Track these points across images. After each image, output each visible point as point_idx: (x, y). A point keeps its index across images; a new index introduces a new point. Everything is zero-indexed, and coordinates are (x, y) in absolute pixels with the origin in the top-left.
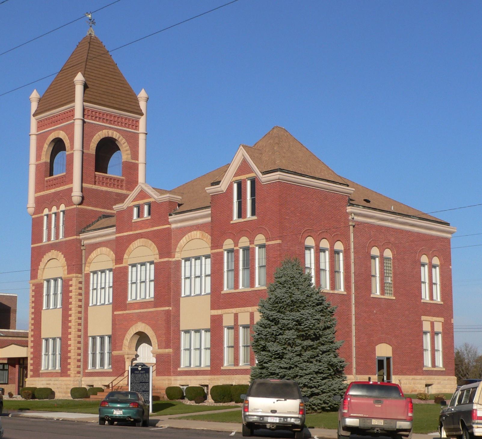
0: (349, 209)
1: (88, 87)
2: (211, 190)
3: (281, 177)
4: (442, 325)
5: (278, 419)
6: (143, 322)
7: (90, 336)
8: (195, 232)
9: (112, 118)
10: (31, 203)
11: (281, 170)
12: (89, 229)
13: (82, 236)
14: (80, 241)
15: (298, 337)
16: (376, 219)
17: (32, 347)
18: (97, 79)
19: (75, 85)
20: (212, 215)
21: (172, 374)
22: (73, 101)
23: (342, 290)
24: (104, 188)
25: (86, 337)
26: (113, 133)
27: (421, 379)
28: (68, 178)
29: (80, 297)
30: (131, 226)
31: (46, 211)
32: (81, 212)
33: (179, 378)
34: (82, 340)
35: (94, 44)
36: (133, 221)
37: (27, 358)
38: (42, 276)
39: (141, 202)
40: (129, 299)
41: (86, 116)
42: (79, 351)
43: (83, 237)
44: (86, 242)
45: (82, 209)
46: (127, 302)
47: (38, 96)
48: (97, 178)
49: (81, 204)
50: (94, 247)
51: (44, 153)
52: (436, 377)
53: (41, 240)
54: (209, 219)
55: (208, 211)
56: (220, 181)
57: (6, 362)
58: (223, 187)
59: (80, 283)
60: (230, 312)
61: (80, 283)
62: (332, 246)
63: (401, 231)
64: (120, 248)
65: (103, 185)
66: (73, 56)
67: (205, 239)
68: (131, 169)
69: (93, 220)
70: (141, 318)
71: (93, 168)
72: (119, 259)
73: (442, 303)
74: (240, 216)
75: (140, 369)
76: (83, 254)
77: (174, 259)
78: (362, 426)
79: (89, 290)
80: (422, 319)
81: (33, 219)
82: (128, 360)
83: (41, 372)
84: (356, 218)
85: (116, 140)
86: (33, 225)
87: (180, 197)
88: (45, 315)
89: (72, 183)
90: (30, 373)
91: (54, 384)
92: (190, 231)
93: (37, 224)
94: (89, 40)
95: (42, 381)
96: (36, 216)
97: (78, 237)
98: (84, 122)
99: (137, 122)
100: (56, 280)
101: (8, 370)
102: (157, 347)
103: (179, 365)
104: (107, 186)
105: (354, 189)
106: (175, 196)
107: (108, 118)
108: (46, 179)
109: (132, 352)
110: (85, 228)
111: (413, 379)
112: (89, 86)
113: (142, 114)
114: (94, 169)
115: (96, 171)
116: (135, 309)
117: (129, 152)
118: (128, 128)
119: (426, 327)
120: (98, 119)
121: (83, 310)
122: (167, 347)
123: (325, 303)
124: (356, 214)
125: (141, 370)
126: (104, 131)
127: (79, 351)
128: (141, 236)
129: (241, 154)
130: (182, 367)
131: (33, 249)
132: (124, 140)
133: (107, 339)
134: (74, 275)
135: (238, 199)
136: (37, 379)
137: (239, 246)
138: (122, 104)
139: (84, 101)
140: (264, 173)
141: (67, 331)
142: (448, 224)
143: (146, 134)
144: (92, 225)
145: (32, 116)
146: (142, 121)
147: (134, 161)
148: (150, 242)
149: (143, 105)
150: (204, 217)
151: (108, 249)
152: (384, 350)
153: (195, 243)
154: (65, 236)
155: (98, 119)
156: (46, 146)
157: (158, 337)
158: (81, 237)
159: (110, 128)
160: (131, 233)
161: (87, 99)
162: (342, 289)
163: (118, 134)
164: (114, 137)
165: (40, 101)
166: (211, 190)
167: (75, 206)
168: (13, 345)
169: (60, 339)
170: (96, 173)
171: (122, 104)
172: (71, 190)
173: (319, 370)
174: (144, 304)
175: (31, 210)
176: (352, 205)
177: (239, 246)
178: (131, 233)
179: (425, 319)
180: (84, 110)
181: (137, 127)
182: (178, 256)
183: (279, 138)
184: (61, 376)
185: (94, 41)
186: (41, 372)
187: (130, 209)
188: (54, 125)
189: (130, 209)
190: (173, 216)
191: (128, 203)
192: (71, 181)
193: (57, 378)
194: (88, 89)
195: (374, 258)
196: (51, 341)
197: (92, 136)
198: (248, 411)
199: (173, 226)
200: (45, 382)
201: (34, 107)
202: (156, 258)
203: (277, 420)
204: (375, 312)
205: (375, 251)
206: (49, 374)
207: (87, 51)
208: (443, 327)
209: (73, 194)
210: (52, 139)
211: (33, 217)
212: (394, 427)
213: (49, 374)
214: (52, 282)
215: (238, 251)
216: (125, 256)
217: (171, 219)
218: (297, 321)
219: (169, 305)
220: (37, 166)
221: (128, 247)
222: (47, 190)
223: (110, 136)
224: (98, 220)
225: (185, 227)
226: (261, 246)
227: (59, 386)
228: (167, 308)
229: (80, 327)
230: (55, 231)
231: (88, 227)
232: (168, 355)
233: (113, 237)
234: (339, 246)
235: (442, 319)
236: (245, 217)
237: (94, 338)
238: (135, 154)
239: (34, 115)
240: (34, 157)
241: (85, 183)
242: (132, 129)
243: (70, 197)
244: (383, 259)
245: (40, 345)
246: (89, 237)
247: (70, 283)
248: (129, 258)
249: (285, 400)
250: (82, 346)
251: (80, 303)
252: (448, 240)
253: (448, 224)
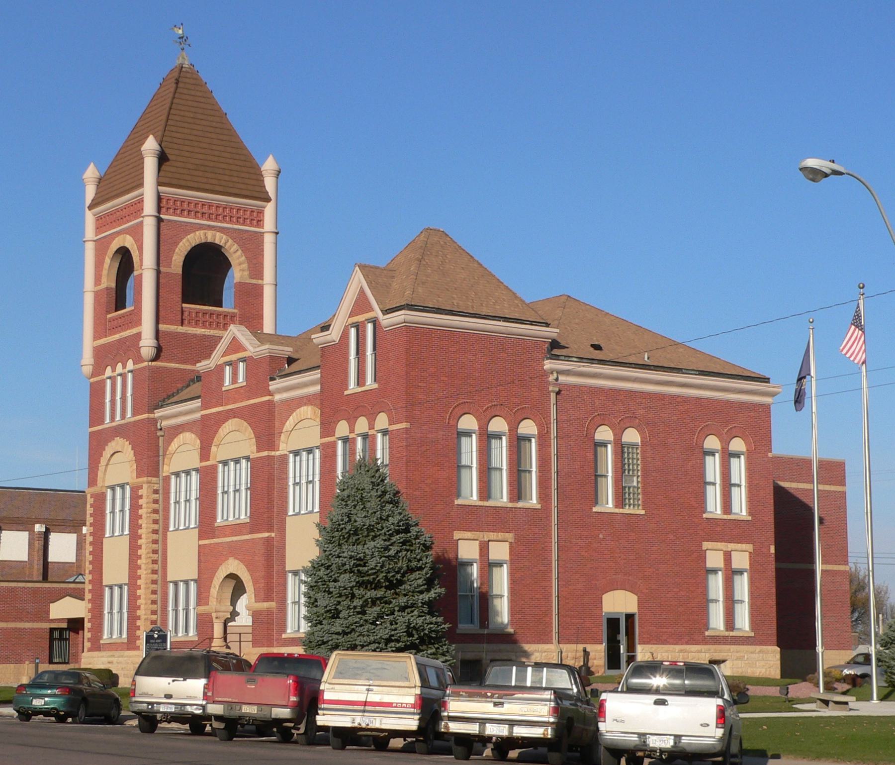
0: (548, 365)
1: (167, 160)
2: (319, 338)
3: (409, 318)
4: (750, 557)
5: (173, 707)
6: (236, 558)
7: (171, 582)
8: (305, 408)
9: (213, 210)
10: (87, 358)
11: (410, 307)
12: (170, 401)
13: (158, 413)
14: (154, 421)
15: (360, 585)
16: (606, 378)
17: (89, 600)
18: (187, 142)
19: (143, 158)
20: (322, 382)
21: (275, 643)
22: (141, 185)
23: (533, 501)
24: (199, 331)
25: (165, 583)
26: (214, 236)
27: (700, 652)
28: (135, 319)
29: (156, 516)
30: (220, 397)
31: (109, 372)
32: (155, 371)
34: (158, 587)
35: (187, 80)
36: (224, 389)
37: (83, 619)
38: (104, 481)
39: (234, 357)
40: (219, 520)
41: (163, 210)
42: (154, 607)
43: (160, 414)
44: (165, 423)
45: (158, 368)
46: (216, 525)
47: (97, 175)
48: (186, 314)
49: (156, 358)
50: (177, 430)
51: (105, 272)
52: (733, 648)
53: (101, 421)
54: (317, 388)
55: (316, 375)
56: (330, 326)
57: (65, 625)
58: (334, 334)
59: (156, 492)
61: (156, 492)
62: (513, 428)
63: (661, 397)
64: (207, 431)
65: (197, 325)
66: (155, 102)
68: (251, 295)
69: (180, 386)
70: (234, 551)
71: (178, 297)
72: (205, 453)
73: (750, 518)
75: (156, 636)
77: (278, 453)
78: (227, 714)
79: (169, 503)
80: (704, 548)
81: (91, 384)
82: (218, 621)
83: (102, 642)
84: (562, 379)
85: (221, 247)
86: (92, 395)
87: (291, 349)
88: (108, 545)
89: (141, 325)
90: (87, 645)
91: (118, 663)
92: (299, 406)
93: (97, 392)
94: (176, 75)
95: (102, 657)
97: (151, 416)
98: (159, 220)
99: (261, 212)
100: (122, 486)
101: (68, 639)
103: (283, 628)
104: (204, 326)
105: (558, 331)
106: (281, 348)
107: (205, 210)
108: (109, 316)
109: (223, 608)
110: (164, 400)
111: (681, 651)
112: (169, 157)
113: (268, 200)
114: (180, 300)
115: (184, 301)
116: (225, 536)
117: (245, 266)
118: (243, 224)
119: (714, 559)
120: (186, 213)
121: (159, 537)
122: (268, 599)
123: (414, 530)
124: (560, 372)
125: (158, 638)
126: (197, 233)
127: (154, 607)
129: (358, 280)
130: (289, 631)
131: (92, 434)
132: (235, 247)
133: (193, 586)
134: (145, 479)
136: (96, 653)
137: (337, 435)
138: (231, 185)
139: (159, 184)
140: (386, 312)
142: (766, 380)
143: (277, 233)
144: (178, 393)
145: (87, 209)
146: (269, 210)
147: (254, 281)
148: (245, 424)
149: (269, 184)
150: (309, 383)
151: (193, 436)
152: (619, 602)
153: (302, 430)
154: (134, 415)
155: (186, 213)
156: (108, 260)
157: (255, 582)
158: (156, 415)
159: (210, 228)
160: (220, 409)
161: (163, 180)
162: (534, 501)
163: (224, 237)
164: (217, 242)
165: (100, 181)
166: (319, 338)
167: (146, 364)
168: (68, 598)
169: (195, 581)
170: (184, 305)
171: (231, 185)
172: (138, 336)
173: (393, 635)
174: (237, 529)
175: (87, 370)
176: (557, 357)
177: (337, 435)
178: (220, 409)
179: (710, 547)
180: (159, 199)
181: (260, 222)
182: (283, 448)
183: (433, 248)
184: (128, 649)
185: (188, 75)
186: (102, 642)
187: (220, 369)
188: (128, 221)
189: (220, 369)
190: (277, 381)
191: (216, 358)
192: (138, 322)
193: (122, 653)
194: (167, 163)
195: (604, 444)
196: (182, 586)
197: (176, 244)
198: (134, 696)
199: (277, 397)
200: (105, 660)
201: (90, 192)
203: (172, 709)
204: (601, 536)
205: (604, 433)
206: (113, 646)
207: (171, 95)
208: (750, 560)
209: (141, 343)
210: (115, 249)
211: (92, 380)
212: (268, 716)
213: (113, 646)
214: (118, 490)
215: (354, 440)
216: (214, 449)
217: (273, 386)
218: (360, 559)
219: (270, 530)
220: (97, 294)
221: (216, 432)
222: (110, 335)
223: (209, 240)
224: (188, 386)
226: (385, 432)
227: (124, 666)
228: (266, 535)
229: (156, 567)
230: (122, 406)
231: (169, 397)
232: (269, 612)
233: (198, 415)
234: (528, 427)
235: (749, 547)
237: (176, 584)
238: (257, 270)
239: (91, 207)
240: (92, 279)
241: (164, 323)
242: (251, 225)
243: (138, 348)
244: (621, 449)
245: (101, 596)
246: (170, 415)
247: (140, 492)
248: (219, 452)
249: (185, 680)
250: (158, 597)
251: (156, 527)
252: (766, 408)
253: (766, 380)
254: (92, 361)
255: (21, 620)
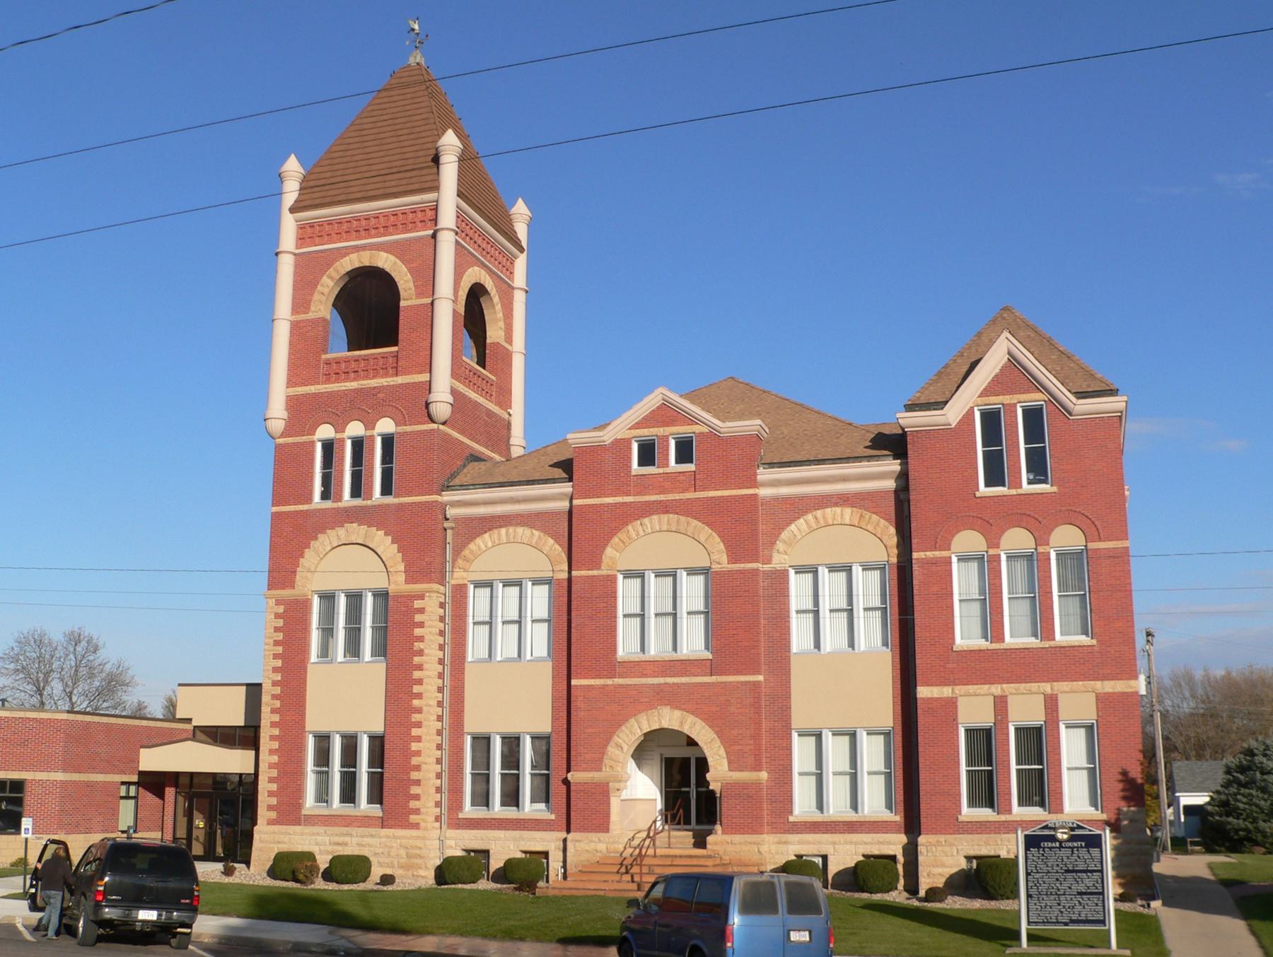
10: (277, 410)
13: (447, 497)
14: (443, 507)
33: (791, 837)
52: (501, 834)
58: (952, 414)
60: (982, 692)
67: (869, 528)
74: (325, 495)
76: (449, 539)
77: (767, 567)
96: (290, 440)
102: (726, 767)
128: (665, 508)
131: (276, 517)
135: (384, 461)
140: (1081, 395)
141: (409, 717)
146: (521, 264)
149: (521, 231)
159: (364, 248)
164: (380, 265)
175: (277, 426)
182: (779, 560)
193: (372, 831)
199: (764, 492)
202: (720, 560)
209: (433, 397)
216: (609, 551)
225: (802, 498)
236: (370, 496)
254: (285, 415)
255: (93, 769)
